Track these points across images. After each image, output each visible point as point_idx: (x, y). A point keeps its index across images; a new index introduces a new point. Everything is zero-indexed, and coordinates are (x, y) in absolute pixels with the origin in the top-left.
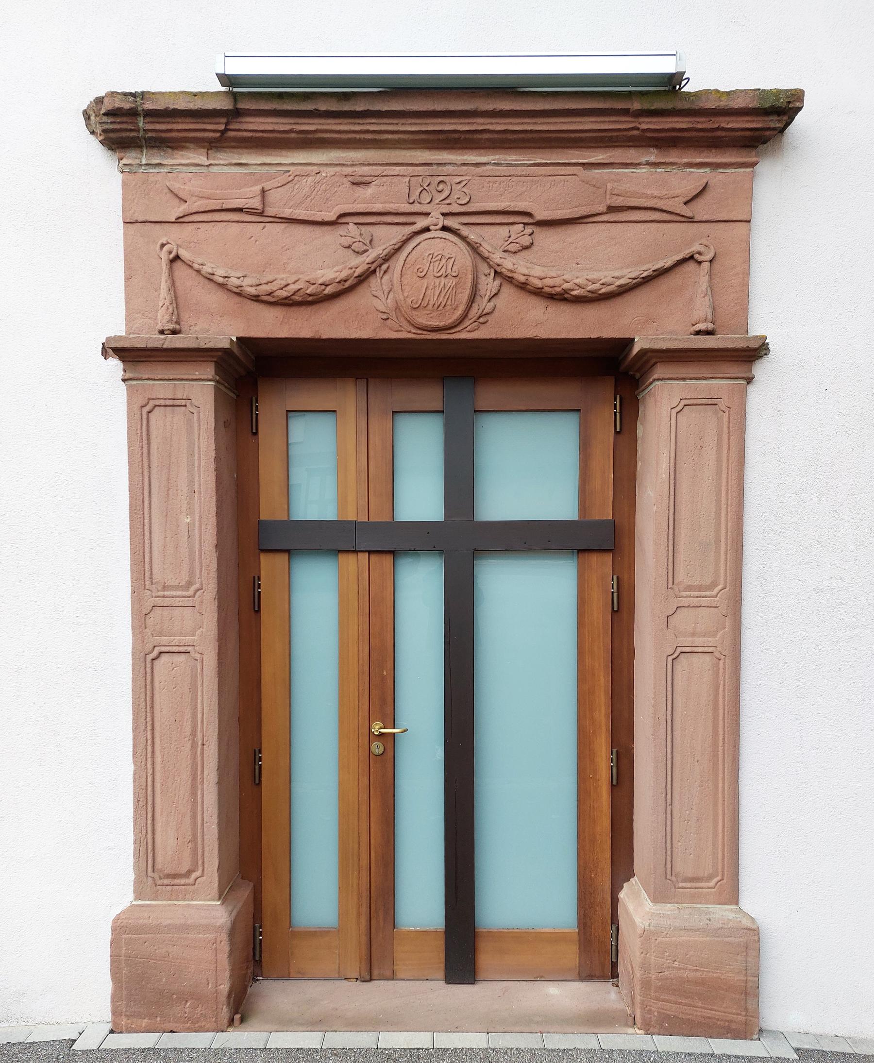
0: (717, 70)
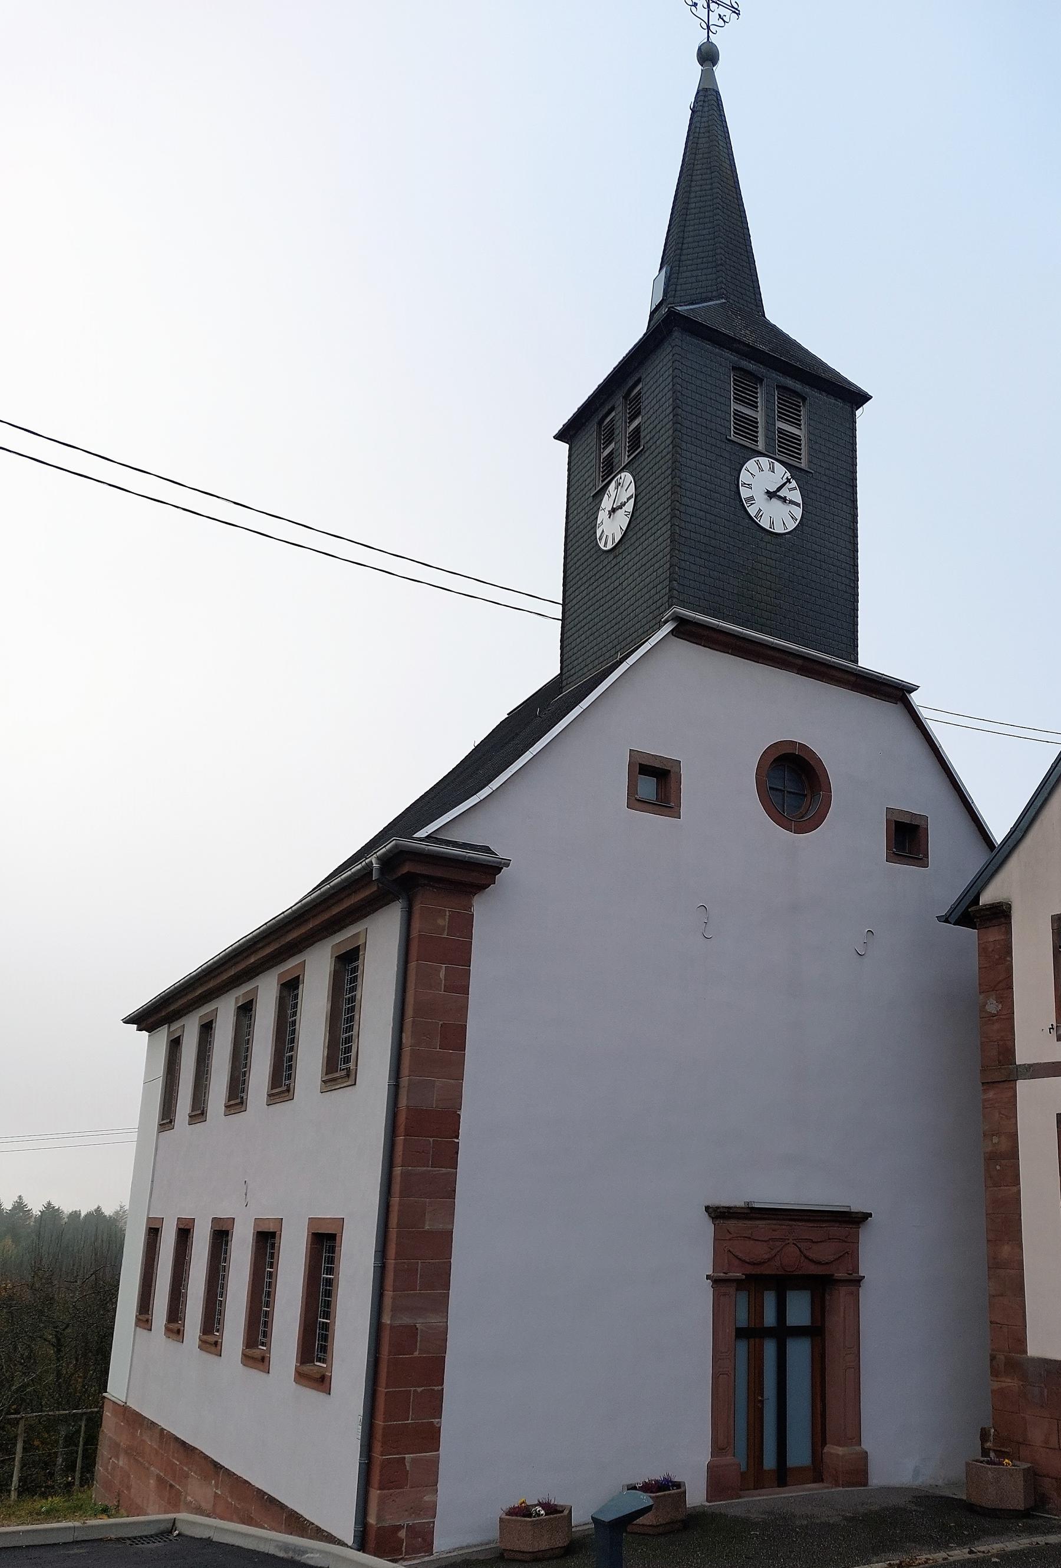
0: (856, 1207)
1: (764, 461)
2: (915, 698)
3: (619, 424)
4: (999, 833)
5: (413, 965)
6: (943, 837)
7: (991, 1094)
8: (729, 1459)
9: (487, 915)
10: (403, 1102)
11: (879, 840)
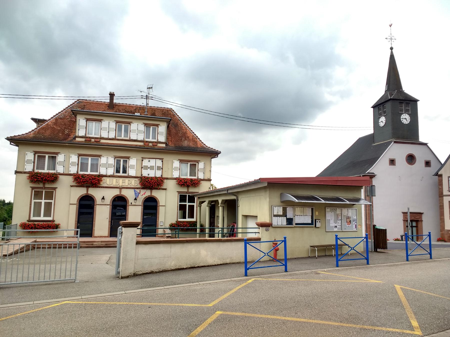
0: (422, 212)
1: (404, 114)
4: (443, 163)
9: (375, 182)
11: (424, 164)
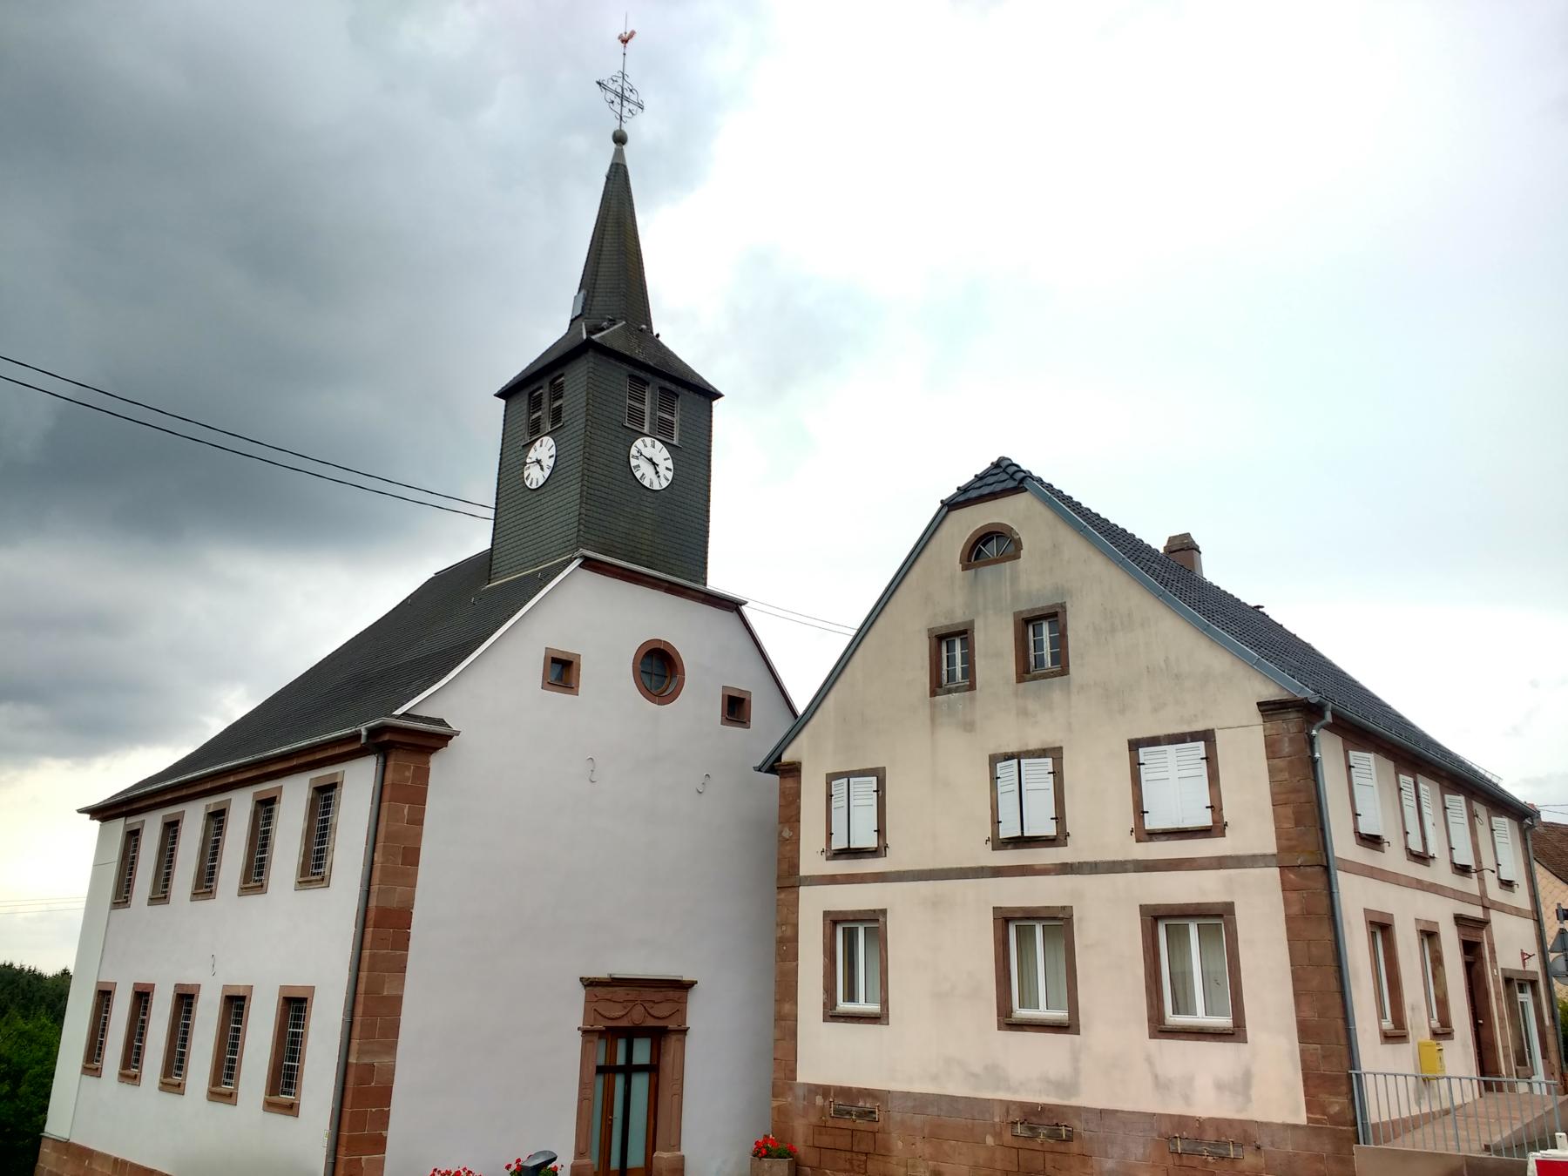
0: (687, 978)
1: (648, 440)
2: (744, 609)
3: (545, 399)
4: (800, 708)
5: (385, 805)
6: (761, 708)
7: (782, 896)
8: (586, 1161)
10: (373, 903)
11: (717, 708)
